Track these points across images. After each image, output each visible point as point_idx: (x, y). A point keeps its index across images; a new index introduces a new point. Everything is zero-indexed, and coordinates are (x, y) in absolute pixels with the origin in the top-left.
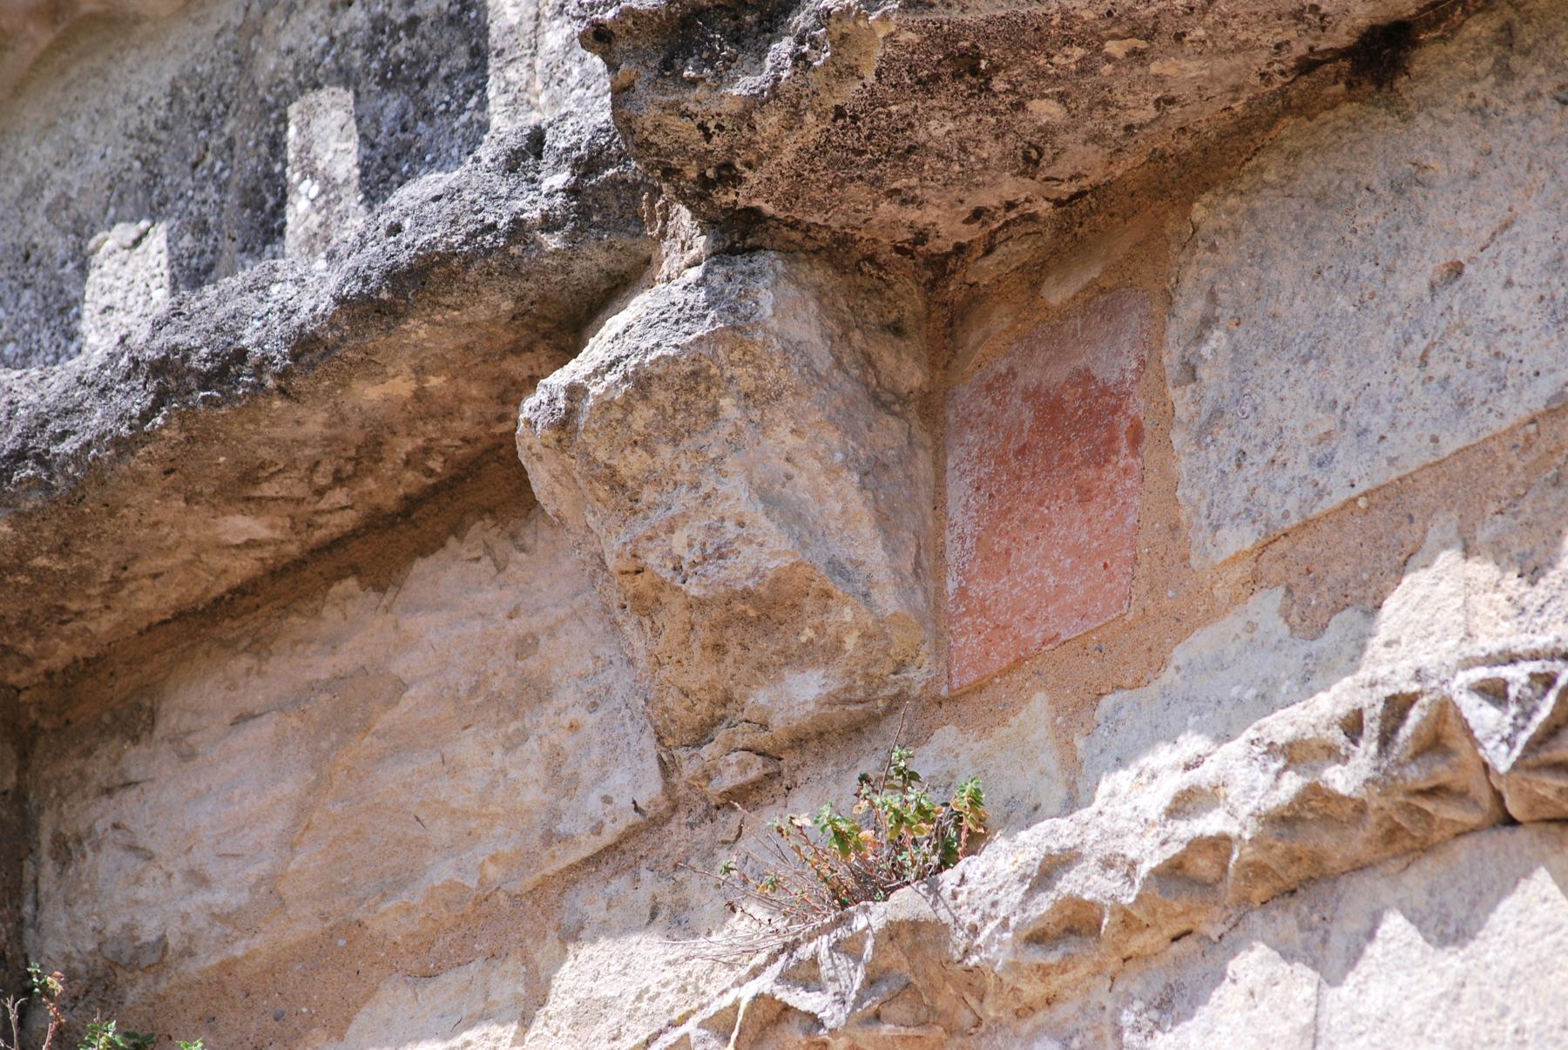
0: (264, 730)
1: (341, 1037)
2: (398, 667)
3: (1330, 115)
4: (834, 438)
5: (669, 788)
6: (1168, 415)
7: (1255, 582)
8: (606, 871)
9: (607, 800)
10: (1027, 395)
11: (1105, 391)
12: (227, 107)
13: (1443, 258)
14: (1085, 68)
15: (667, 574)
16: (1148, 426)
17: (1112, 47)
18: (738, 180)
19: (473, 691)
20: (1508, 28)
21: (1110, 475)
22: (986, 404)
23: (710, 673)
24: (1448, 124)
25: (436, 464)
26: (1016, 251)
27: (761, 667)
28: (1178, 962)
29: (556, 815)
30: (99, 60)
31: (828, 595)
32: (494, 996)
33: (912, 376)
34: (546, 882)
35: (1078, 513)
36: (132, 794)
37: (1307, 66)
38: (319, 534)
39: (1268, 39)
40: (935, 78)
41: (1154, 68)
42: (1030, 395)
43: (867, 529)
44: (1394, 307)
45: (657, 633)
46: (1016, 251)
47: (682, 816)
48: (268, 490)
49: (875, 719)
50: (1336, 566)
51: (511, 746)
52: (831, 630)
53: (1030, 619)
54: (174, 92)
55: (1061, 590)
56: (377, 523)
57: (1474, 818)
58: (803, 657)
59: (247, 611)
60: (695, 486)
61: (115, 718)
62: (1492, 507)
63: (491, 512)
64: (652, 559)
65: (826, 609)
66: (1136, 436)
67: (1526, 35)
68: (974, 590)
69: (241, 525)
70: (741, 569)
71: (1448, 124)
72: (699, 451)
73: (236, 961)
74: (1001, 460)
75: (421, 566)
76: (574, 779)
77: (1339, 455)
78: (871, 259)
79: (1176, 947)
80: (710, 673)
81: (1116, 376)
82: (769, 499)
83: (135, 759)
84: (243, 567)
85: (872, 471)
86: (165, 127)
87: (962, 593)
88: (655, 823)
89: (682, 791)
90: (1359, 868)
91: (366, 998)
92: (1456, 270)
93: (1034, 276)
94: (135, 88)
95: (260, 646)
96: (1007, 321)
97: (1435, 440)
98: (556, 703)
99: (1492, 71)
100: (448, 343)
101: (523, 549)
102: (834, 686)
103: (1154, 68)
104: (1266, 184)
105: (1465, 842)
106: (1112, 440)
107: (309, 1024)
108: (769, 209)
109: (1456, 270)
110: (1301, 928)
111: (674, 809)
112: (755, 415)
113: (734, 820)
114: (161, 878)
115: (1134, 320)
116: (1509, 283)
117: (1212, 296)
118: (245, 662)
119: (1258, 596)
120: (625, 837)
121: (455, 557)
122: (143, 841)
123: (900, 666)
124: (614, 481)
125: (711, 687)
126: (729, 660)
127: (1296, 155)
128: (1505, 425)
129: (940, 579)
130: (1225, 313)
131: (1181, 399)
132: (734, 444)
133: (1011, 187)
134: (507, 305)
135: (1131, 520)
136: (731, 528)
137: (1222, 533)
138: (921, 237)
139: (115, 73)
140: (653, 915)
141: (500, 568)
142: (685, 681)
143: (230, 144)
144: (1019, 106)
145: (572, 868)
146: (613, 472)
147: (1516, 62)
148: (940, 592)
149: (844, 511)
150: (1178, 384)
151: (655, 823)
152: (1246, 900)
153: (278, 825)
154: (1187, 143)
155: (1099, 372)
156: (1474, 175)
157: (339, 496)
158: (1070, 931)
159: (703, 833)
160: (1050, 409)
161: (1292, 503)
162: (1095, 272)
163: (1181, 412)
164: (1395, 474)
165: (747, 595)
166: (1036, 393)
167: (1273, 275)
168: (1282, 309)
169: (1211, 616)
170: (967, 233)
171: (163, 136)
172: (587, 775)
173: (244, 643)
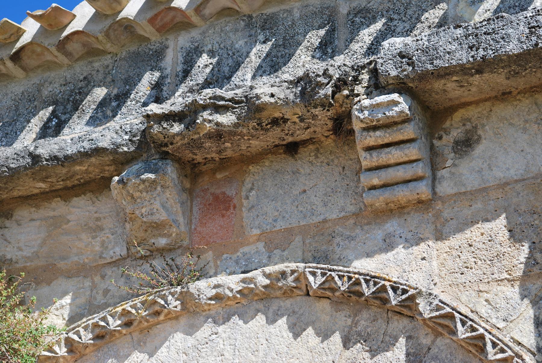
0: (38, 223)
1: (49, 285)
2: (69, 217)
3: (280, 156)
4: (177, 197)
5: (128, 253)
6: (242, 205)
7: (258, 240)
8: (112, 266)
9: (114, 253)
10: (211, 194)
11: (228, 197)
12: (35, 99)
13: (303, 188)
14: (239, 140)
15: (139, 216)
16: (237, 206)
17: (246, 138)
18: (168, 147)
19: (85, 225)
20: (318, 148)
21: (229, 213)
22: (202, 194)
23: (143, 235)
24: (305, 163)
25: (82, 181)
26: (210, 166)
27: (154, 236)
28: (237, 308)
29: (102, 253)
30: (5, 83)
31: (171, 225)
32: (85, 285)
33: (188, 185)
34: (98, 265)
35: (221, 219)
36: (7, 229)
37: (276, 146)
38: (53, 188)
39: (272, 141)
40: (213, 137)
41: (251, 142)
42: (212, 194)
43: (181, 215)
44: (292, 195)
45: (133, 225)
46: (210, 166)
47: (130, 258)
48: (49, 180)
49: (175, 249)
50: (276, 241)
51: (94, 238)
52: (171, 232)
53: (210, 237)
54: (23, 93)
55: (217, 233)
56: (66, 188)
57: (302, 293)
58: (164, 235)
59: (34, 199)
60: (149, 201)
61: (3, 214)
62: (309, 236)
63: (92, 192)
64: (137, 212)
65: (170, 228)
66: (235, 207)
67: (321, 151)
68: (198, 229)
69: (42, 185)
70: (156, 218)
71: (305, 163)
72: (152, 195)
73: (27, 266)
74: (205, 205)
75: (75, 199)
76: (107, 247)
77: (279, 220)
78: (183, 162)
79: (237, 305)
80: (143, 235)
81: (231, 194)
82: (164, 207)
83: (7, 223)
84: (36, 191)
85: (182, 203)
86: (20, 100)
87: (195, 229)
88: (125, 259)
89: (130, 254)
90: (277, 298)
91: (55, 279)
92: (305, 191)
93: (214, 171)
94: (14, 91)
95: (37, 207)
96: (208, 179)
97: (299, 222)
98: (104, 232)
99: (314, 155)
100: (97, 162)
101: (99, 201)
102: (168, 242)
103: (251, 142)
104: (266, 166)
105: (299, 297)
106: (229, 207)
107: (42, 281)
108: (170, 152)
109: (305, 191)
110: (264, 306)
111: (128, 257)
112: (163, 190)
113: (141, 262)
114: (12, 247)
115: (235, 185)
116: (316, 196)
117: (253, 184)
118: (34, 209)
119: (259, 243)
120: (117, 260)
121: (84, 199)
122: (9, 239)
123: (182, 241)
124: (132, 197)
125: (142, 237)
126: (148, 233)
127: (272, 161)
128: (314, 222)
129: (191, 225)
130: (256, 188)
131: (245, 203)
132: (159, 195)
133: (214, 155)
134: (112, 158)
135: (233, 223)
136: (155, 210)
137: (253, 230)
138: (193, 160)
139: (9, 87)
140: (122, 276)
141: (93, 203)
142: (136, 235)
143: (36, 107)
144: (224, 143)
145: (105, 264)
146: (133, 195)
147: (319, 155)
148: (191, 228)
149: (176, 210)
150: (244, 199)
151: (125, 259)
152: (253, 299)
153: (39, 242)
154: (249, 154)
155: (227, 193)
156: (309, 174)
157: (61, 183)
158: (216, 298)
159: (134, 262)
160: (216, 198)
161: (268, 227)
162: (227, 174)
163: (245, 204)
164: (290, 226)
165: (155, 223)
166: (213, 194)
167: (266, 183)
168: (268, 190)
169: (248, 244)
170: (201, 160)
171: (20, 101)
172: (110, 247)
173: (34, 205)
